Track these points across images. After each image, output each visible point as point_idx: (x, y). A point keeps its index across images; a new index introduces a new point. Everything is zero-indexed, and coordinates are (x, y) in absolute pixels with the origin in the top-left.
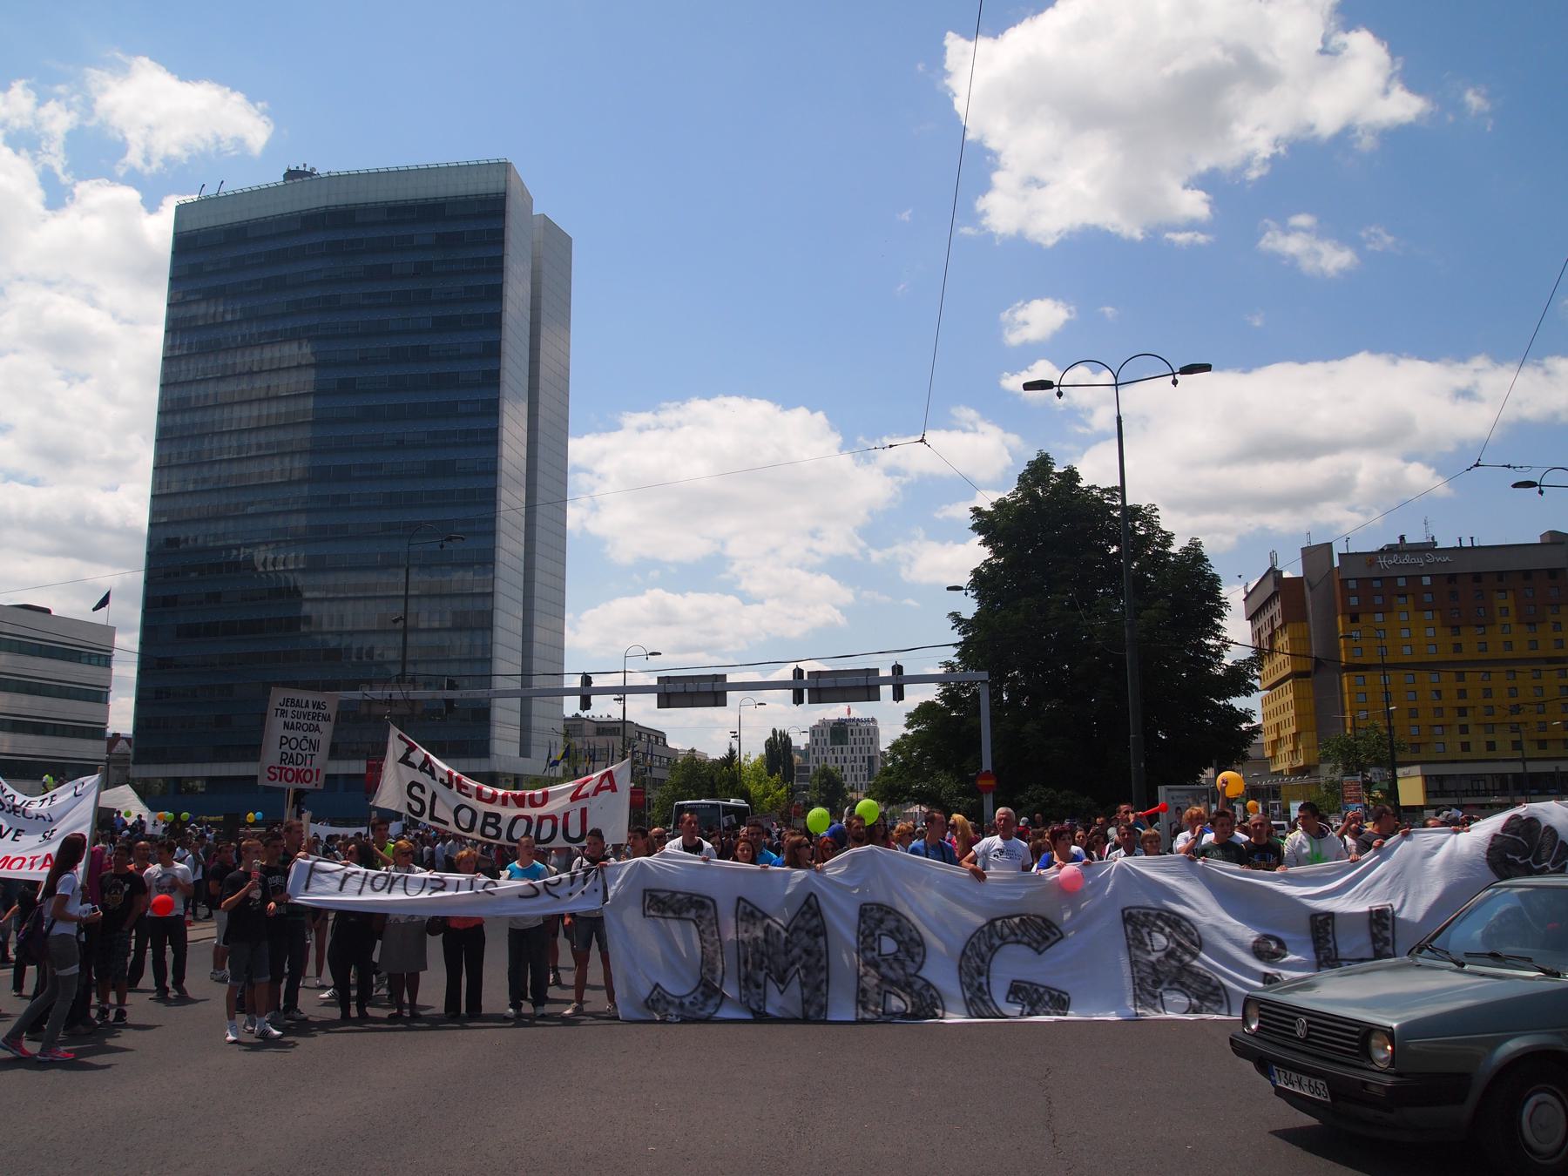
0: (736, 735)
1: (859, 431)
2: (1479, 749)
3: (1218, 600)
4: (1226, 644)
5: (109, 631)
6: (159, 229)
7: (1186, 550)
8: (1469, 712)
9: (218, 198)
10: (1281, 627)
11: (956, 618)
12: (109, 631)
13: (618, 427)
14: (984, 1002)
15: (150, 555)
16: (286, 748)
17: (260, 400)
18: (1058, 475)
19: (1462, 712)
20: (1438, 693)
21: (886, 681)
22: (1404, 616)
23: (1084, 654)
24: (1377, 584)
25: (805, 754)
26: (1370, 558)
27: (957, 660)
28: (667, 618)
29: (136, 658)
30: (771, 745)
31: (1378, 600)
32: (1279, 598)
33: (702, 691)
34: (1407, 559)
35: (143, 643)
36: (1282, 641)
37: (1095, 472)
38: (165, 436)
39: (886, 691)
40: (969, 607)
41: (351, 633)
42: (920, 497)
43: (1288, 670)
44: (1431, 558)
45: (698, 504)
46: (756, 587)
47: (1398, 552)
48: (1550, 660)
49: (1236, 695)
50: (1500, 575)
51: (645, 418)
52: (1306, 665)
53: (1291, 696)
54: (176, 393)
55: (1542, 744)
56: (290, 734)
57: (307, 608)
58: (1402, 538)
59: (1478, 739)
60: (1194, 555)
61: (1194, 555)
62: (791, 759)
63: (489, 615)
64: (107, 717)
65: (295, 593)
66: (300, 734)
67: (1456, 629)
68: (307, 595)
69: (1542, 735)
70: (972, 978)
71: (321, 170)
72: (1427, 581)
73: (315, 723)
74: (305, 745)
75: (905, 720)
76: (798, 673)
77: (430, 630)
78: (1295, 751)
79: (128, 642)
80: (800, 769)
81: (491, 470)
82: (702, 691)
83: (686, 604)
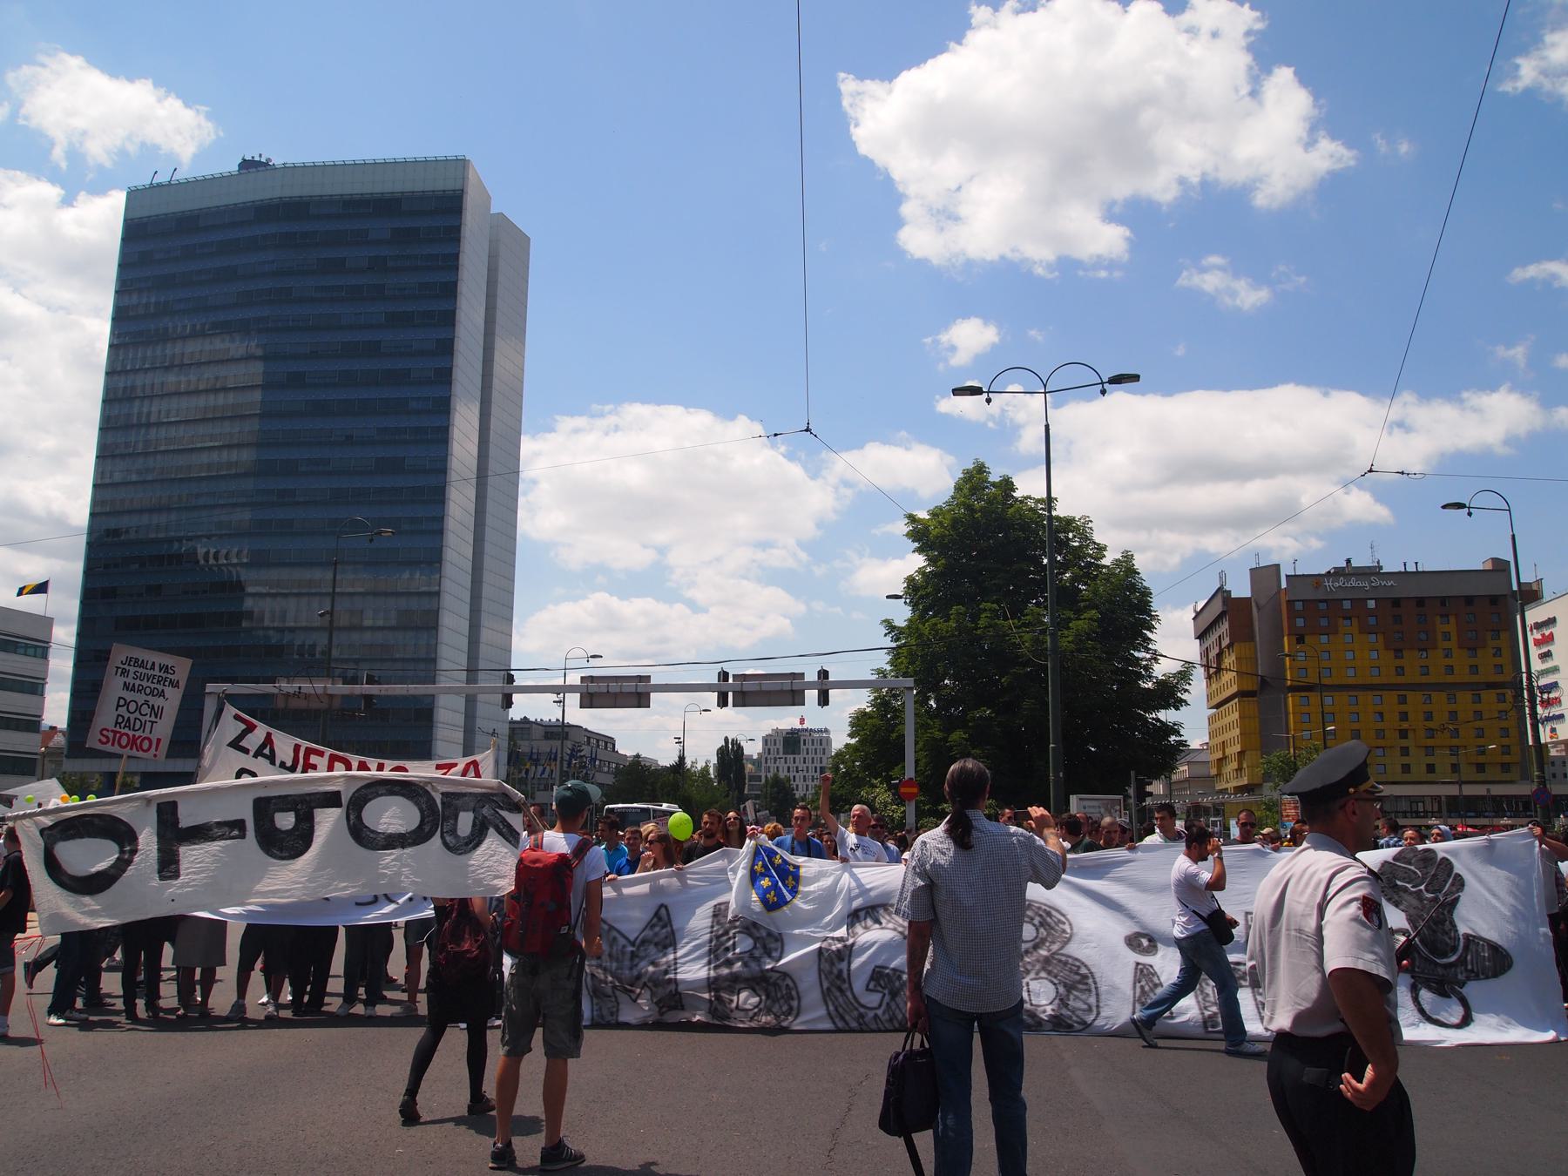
0: (680, 741)
1: (805, 435)
2: (1419, 771)
3: (1148, 613)
4: (1156, 657)
5: (47, 622)
6: (100, 220)
7: (1117, 563)
8: (1410, 735)
9: (169, 184)
10: (1228, 647)
11: (890, 627)
12: (47, 622)
13: (551, 429)
14: (840, 990)
15: (89, 545)
16: (122, 710)
17: (207, 391)
18: (994, 484)
19: (1403, 734)
20: (1381, 714)
21: (811, 686)
22: (1348, 639)
23: (1016, 661)
24: (1322, 606)
25: (757, 763)
26: (1316, 580)
27: (888, 668)
28: (613, 624)
29: (73, 652)
30: (722, 752)
31: (1324, 622)
32: (1227, 619)
33: (632, 692)
34: (1353, 582)
35: (80, 635)
36: (1230, 660)
37: (1029, 486)
38: (108, 426)
39: (812, 695)
40: (902, 614)
41: (292, 630)
42: (866, 503)
43: (1234, 689)
44: (1376, 582)
45: (636, 510)
46: (697, 594)
47: (1345, 575)
48: (1491, 686)
49: (1166, 707)
50: (1443, 600)
51: (580, 421)
52: (1250, 685)
53: (1236, 715)
54: (121, 382)
55: (1481, 768)
56: (129, 696)
57: (249, 603)
58: (1348, 561)
59: (1418, 761)
60: (1126, 565)
61: (1126, 565)
62: (742, 767)
63: (435, 614)
64: (42, 709)
65: (237, 587)
66: (141, 698)
67: (1398, 653)
68: (250, 590)
69: (1481, 759)
70: (832, 964)
71: (277, 161)
72: (1371, 604)
73: (160, 687)
74: (145, 710)
75: (848, 730)
76: (724, 676)
77: (372, 629)
78: (1240, 769)
79: (65, 635)
80: (752, 778)
81: (440, 468)
82: (632, 692)
83: (633, 608)
